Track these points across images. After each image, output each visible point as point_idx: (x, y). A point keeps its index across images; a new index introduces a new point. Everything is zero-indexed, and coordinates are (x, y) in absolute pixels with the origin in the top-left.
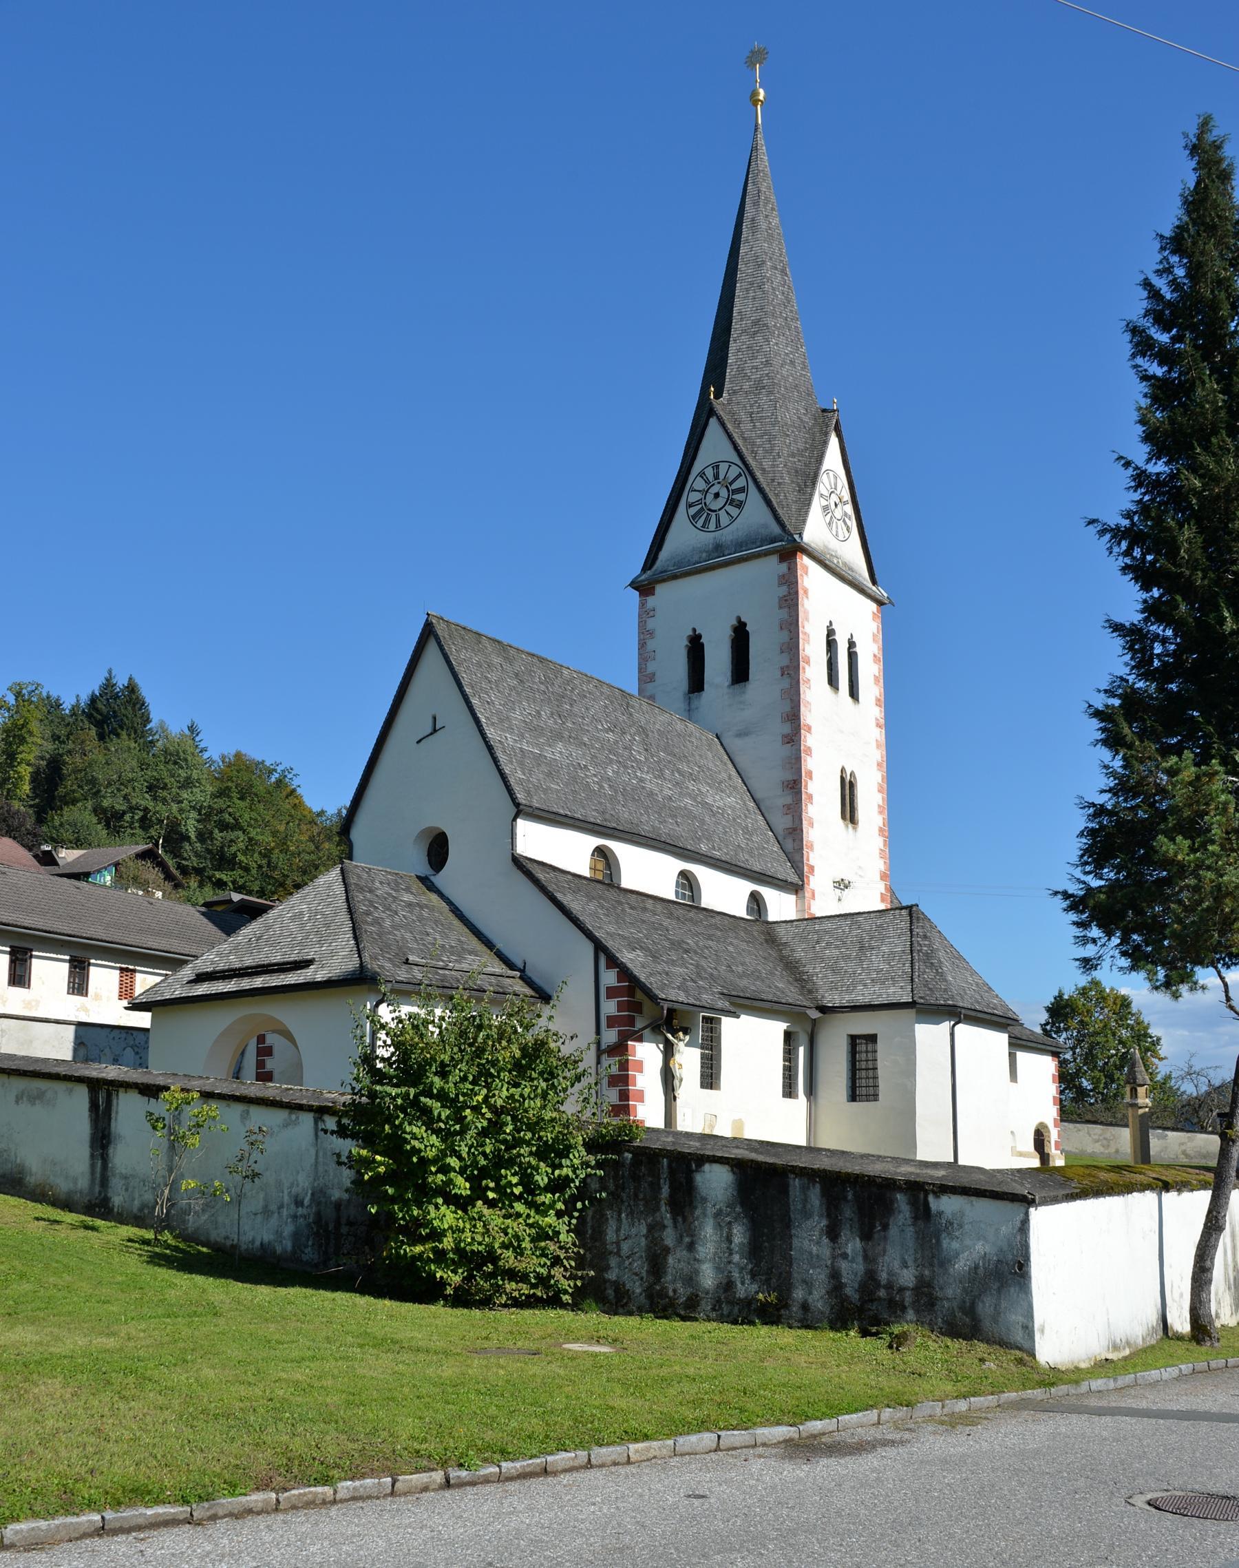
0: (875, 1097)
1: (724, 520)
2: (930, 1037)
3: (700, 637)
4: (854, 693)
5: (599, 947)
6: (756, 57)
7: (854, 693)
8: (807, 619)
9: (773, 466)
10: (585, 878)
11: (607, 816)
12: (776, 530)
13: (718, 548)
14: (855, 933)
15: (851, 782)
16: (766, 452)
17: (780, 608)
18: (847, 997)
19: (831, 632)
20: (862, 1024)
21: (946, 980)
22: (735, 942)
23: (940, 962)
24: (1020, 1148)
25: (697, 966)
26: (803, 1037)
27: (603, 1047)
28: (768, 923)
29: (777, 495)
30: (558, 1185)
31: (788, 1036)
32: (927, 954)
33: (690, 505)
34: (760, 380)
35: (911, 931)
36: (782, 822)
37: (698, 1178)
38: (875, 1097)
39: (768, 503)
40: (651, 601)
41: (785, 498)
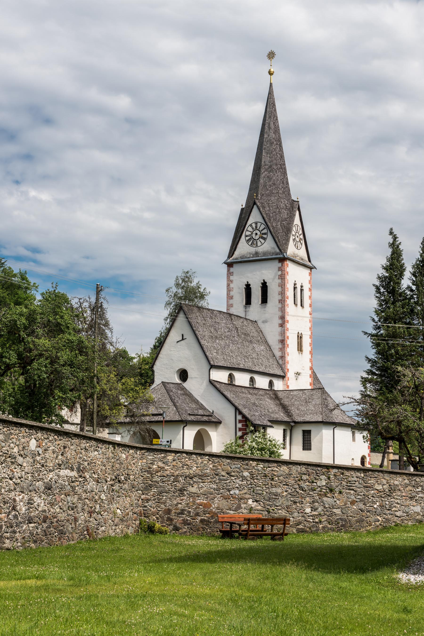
1: (259, 244)
2: (326, 433)
3: (250, 285)
5: (236, 409)
8: (288, 283)
9: (277, 225)
12: (278, 251)
14: (304, 396)
15: (301, 337)
17: (279, 279)
18: (302, 419)
25: (261, 411)
31: (284, 430)
33: (246, 236)
40: (232, 270)
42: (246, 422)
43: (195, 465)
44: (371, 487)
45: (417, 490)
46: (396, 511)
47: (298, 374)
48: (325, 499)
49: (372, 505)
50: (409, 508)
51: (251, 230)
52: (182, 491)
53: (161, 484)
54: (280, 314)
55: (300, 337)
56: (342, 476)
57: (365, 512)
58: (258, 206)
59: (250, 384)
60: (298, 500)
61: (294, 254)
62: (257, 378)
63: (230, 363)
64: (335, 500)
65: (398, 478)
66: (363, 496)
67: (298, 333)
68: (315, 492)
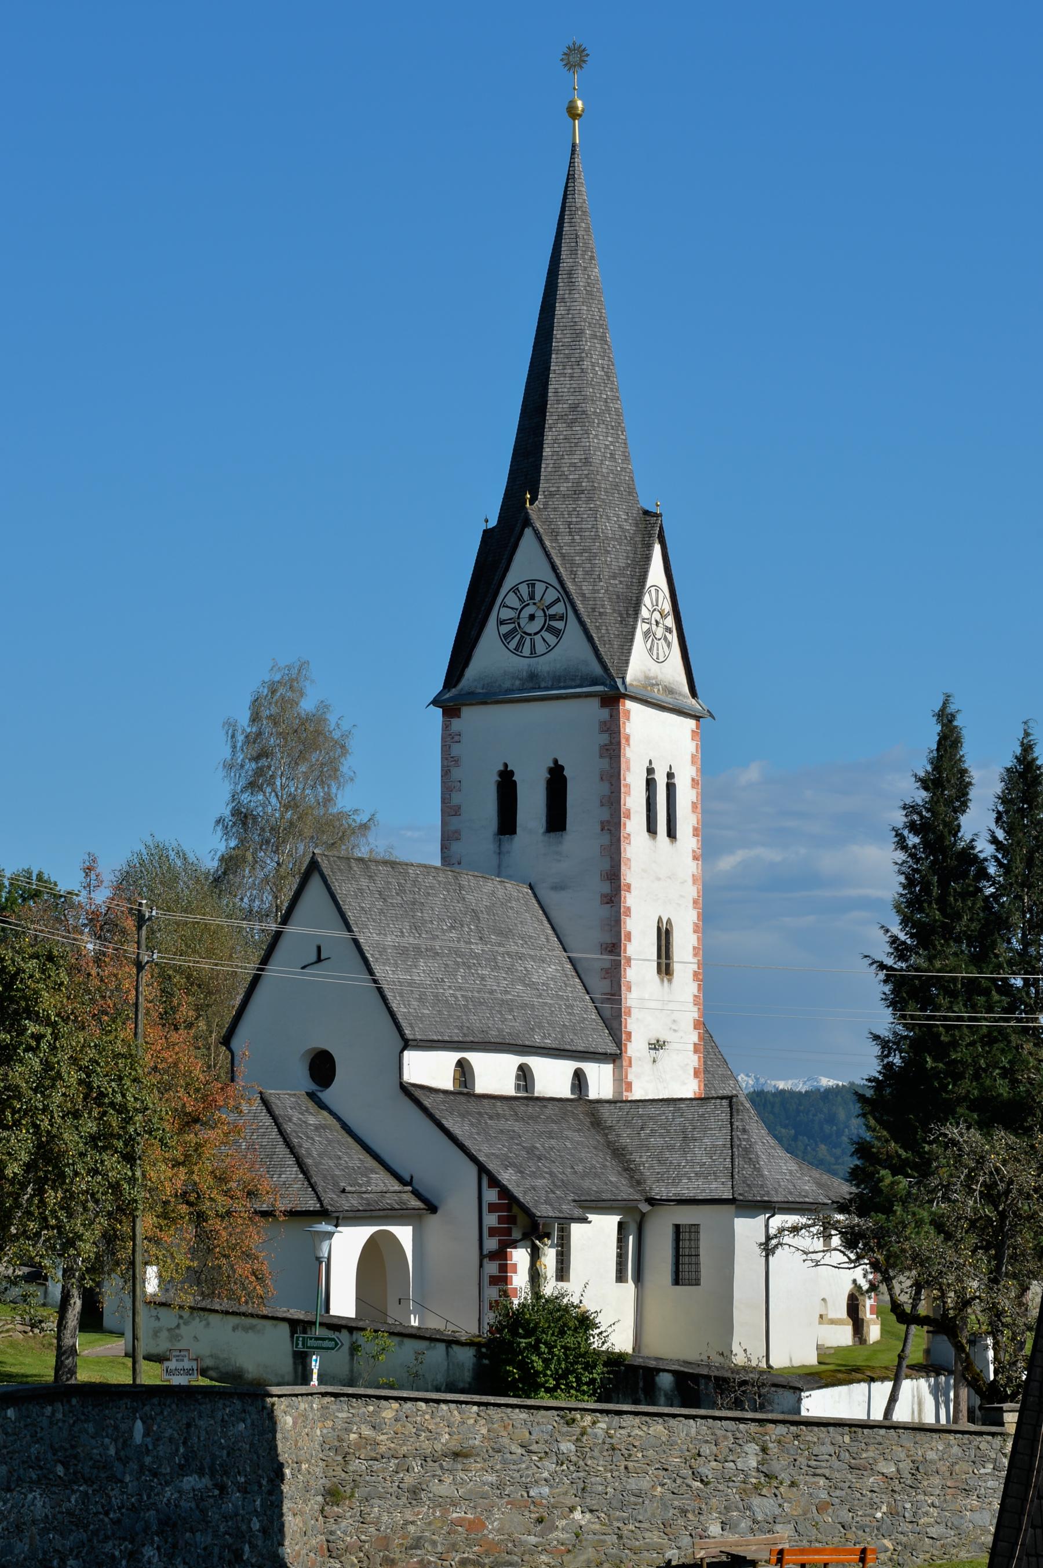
0: (697, 1282)
1: (541, 647)
2: (748, 1230)
3: (512, 773)
4: (671, 834)
5: (482, 1170)
6: (575, 58)
7: (671, 834)
8: (628, 769)
10: (446, 1092)
11: (465, 1030)
12: (598, 670)
13: (533, 680)
14: (678, 1120)
16: (587, 573)
18: (673, 1190)
19: (650, 771)
20: (685, 1216)
21: (762, 1176)
22: (569, 1133)
23: (758, 1156)
24: (832, 1315)
25: (551, 1174)
26: (633, 1227)
27: (485, 1252)
28: (591, 1101)
29: (598, 628)
30: (592, 1381)
31: (620, 1225)
32: (745, 1149)
33: (502, 623)
34: (579, 483)
35: (731, 1124)
36: (599, 986)
37: (657, 1379)
38: (697, 1282)
39: (590, 639)
40: (456, 724)
41: (606, 631)
42: (509, 1210)
43: (447, 1430)
44: (870, 1468)
45: (982, 1471)
46: (930, 1525)
47: (657, 1046)
48: (756, 1501)
49: (869, 1511)
50: (962, 1517)
51: (517, 604)
52: (415, 1493)
53: (368, 1478)
54: (607, 866)
55: (664, 937)
56: (796, 1443)
57: (854, 1529)
58: (536, 532)
59: (518, 1088)
60: (691, 1504)
61: (647, 678)
62: (538, 1064)
63: (460, 1028)
64: (780, 1501)
65: (934, 1444)
66: (849, 1491)
67: (660, 920)
68: (731, 1484)
